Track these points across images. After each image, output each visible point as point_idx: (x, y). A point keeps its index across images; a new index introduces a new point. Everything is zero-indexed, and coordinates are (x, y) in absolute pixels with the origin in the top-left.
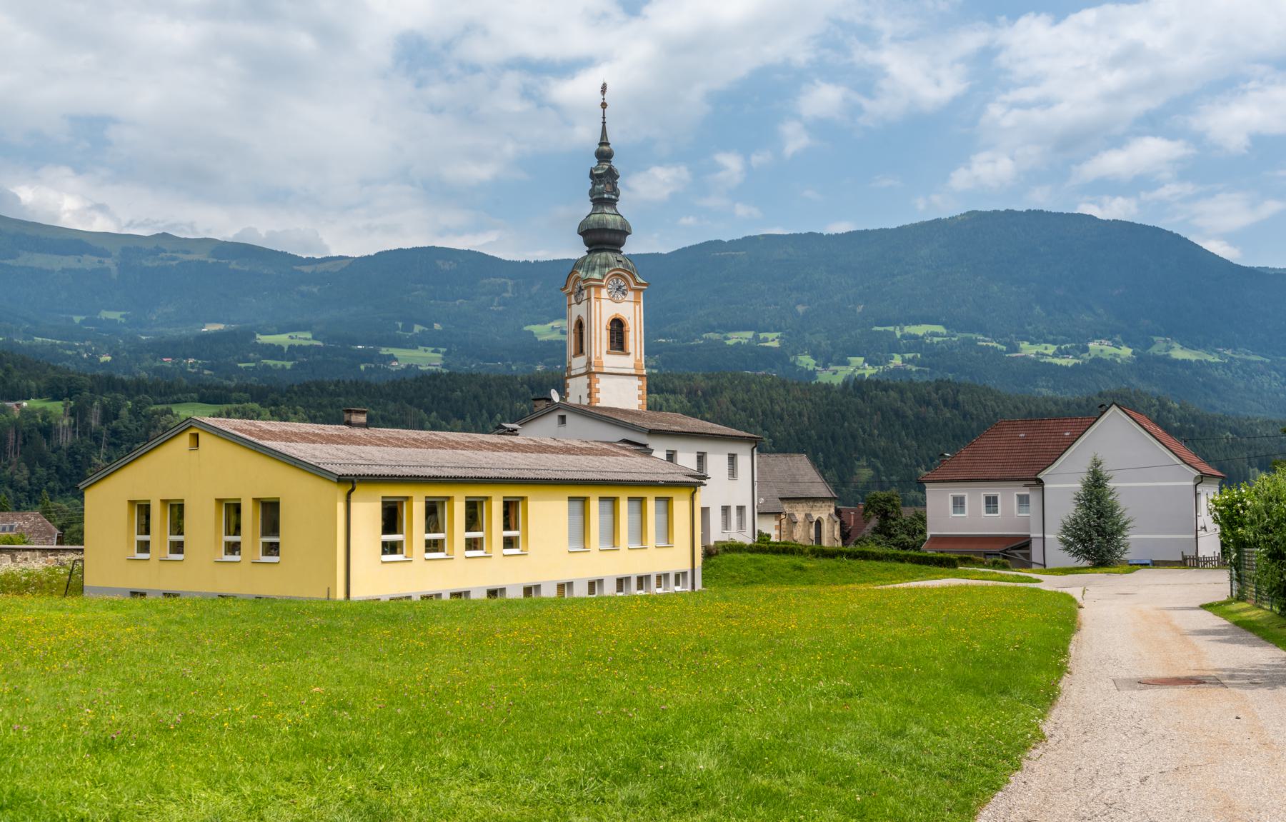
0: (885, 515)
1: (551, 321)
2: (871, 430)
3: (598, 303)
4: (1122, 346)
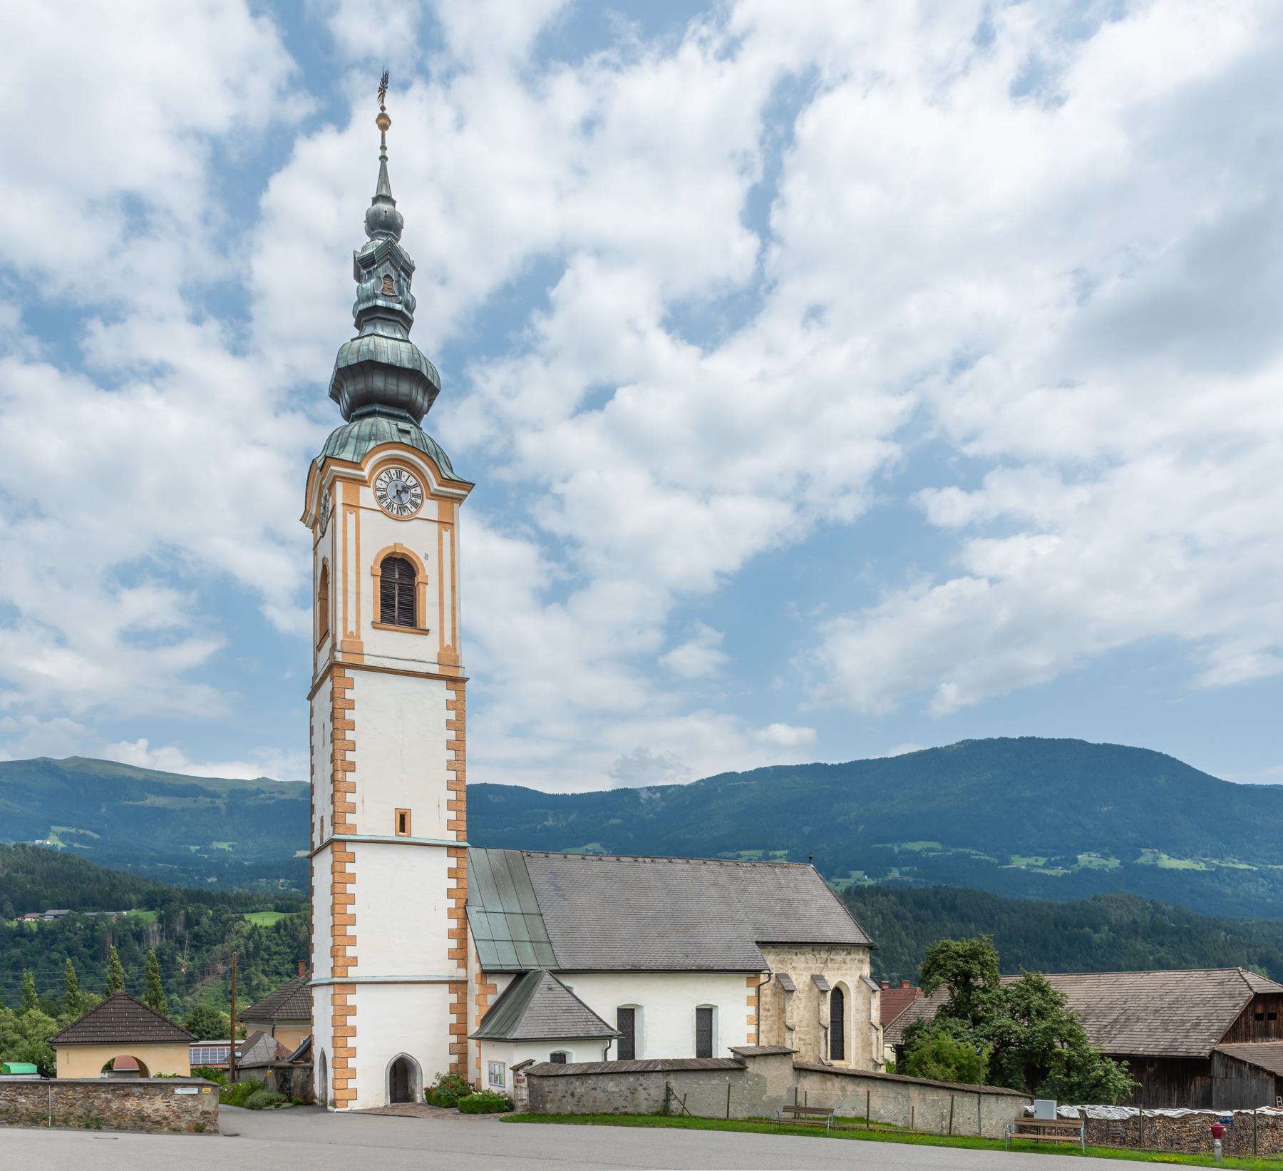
0: (963, 980)
1: (585, 844)
2: (872, 931)
3: (351, 518)
4: (1110, 857)
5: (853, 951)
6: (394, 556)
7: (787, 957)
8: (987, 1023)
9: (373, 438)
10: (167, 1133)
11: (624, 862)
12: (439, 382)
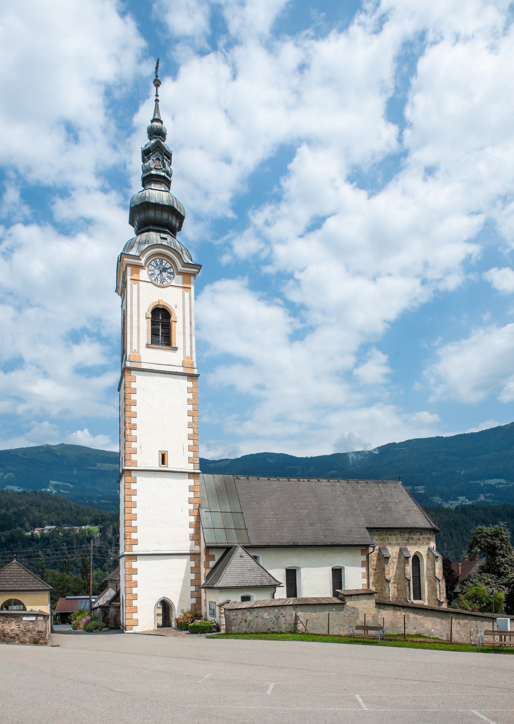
3: (135, 287)
5: (424, 533)
6: (159, 307)
7: (385, 537)
8: (505, 576)
9: (147, 243)
10: (18, 644)
11: (292, 481)
12: (184, 212)
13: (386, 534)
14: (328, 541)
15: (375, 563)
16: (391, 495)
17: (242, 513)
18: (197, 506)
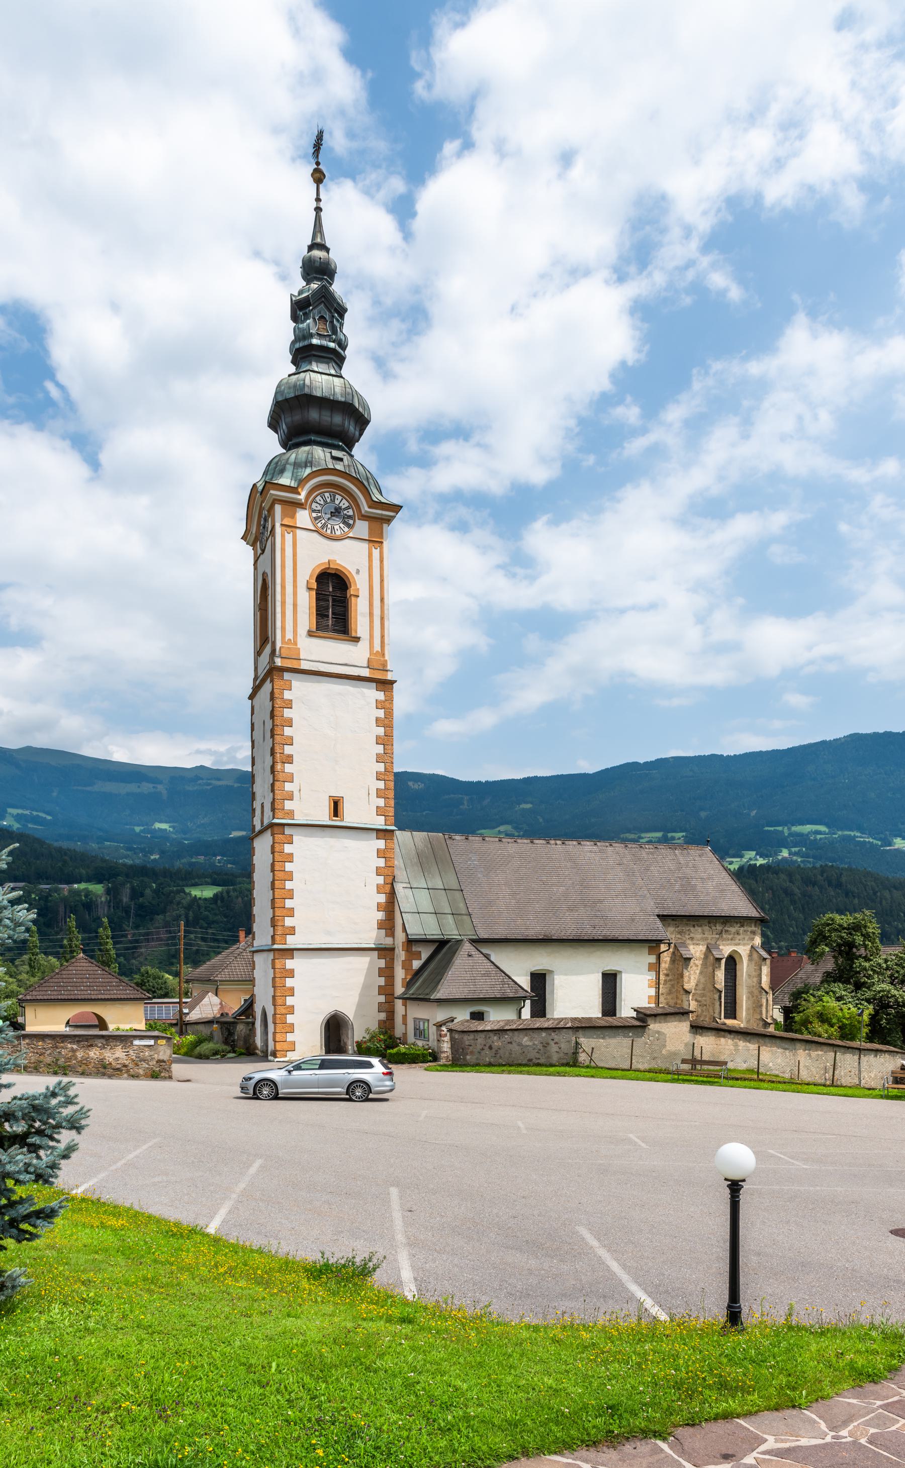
1: (498, 826)
3: (289, 537)
13: (687, 925)
14: (598, 934)
15: (667, 966)
16: (693, 867)
17: (462, 891)
18: (390, 880)
